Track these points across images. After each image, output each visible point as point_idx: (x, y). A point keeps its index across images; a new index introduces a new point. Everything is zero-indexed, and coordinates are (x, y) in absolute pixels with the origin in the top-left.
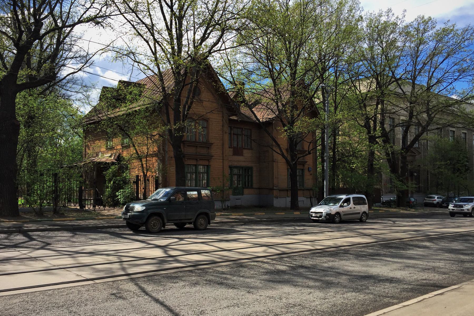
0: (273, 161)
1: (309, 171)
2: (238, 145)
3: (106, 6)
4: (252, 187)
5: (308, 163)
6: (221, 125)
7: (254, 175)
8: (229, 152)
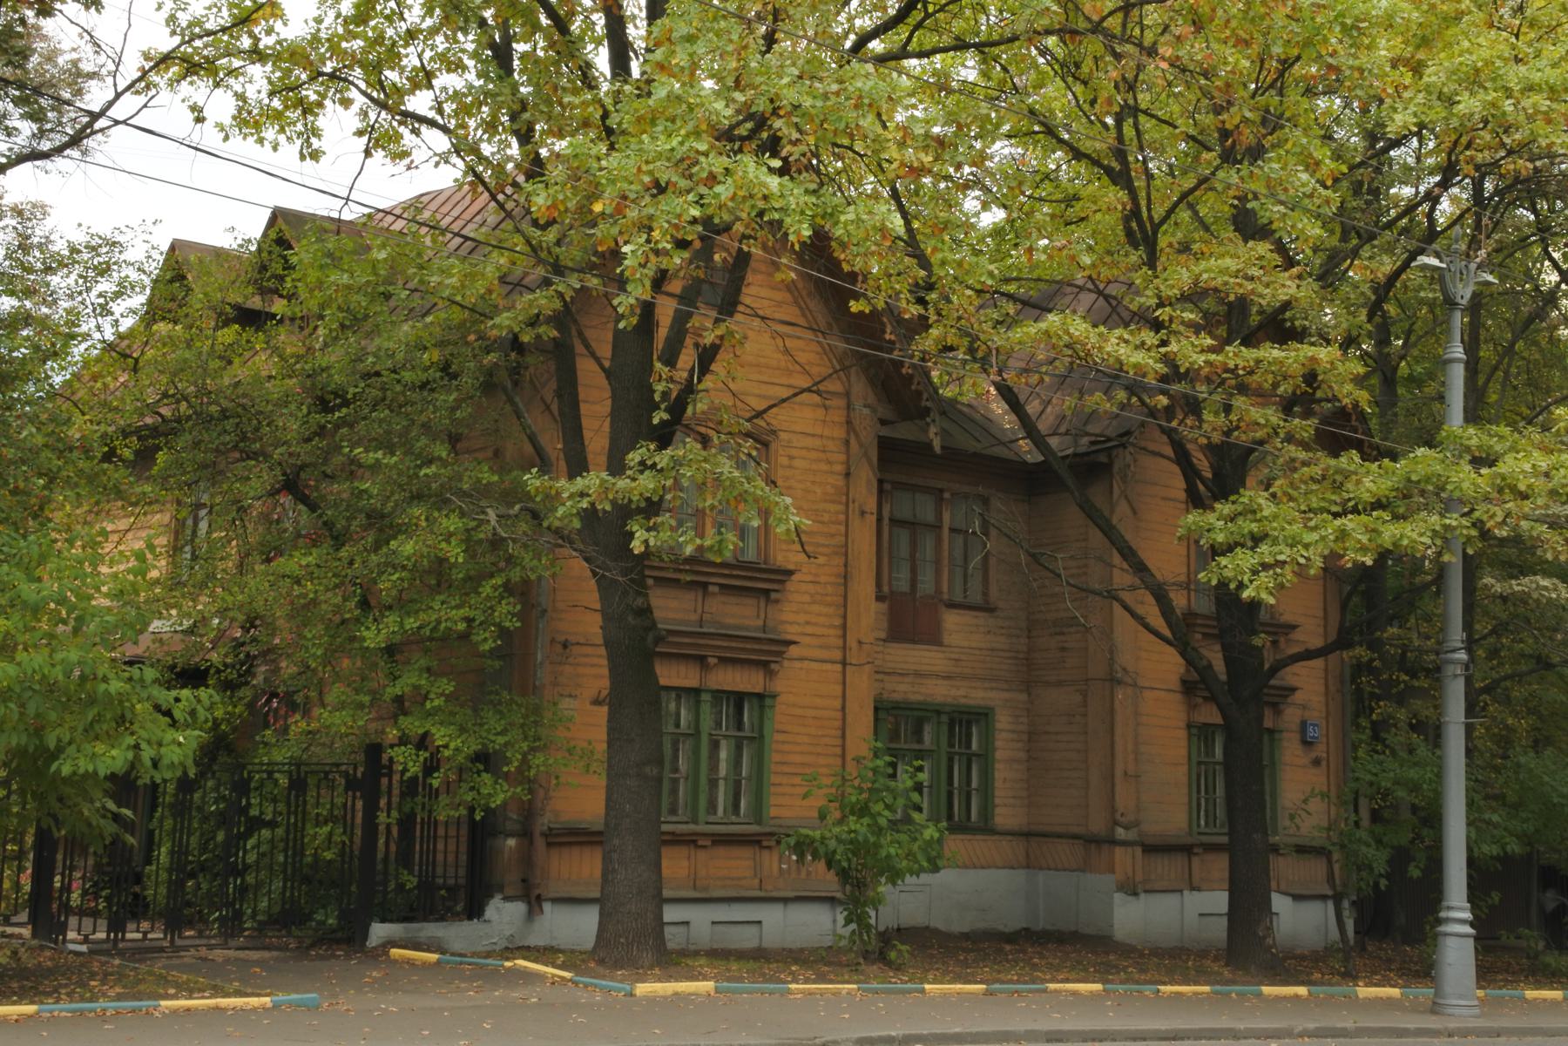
0: (1113, 681)
1: (1307, 743)
2: (914, 583)
3: (1142, 118)
4: (986, 828)
5: (1298, 697)
6: (839, 468)
7: (998, 755)
8: (869, 616)
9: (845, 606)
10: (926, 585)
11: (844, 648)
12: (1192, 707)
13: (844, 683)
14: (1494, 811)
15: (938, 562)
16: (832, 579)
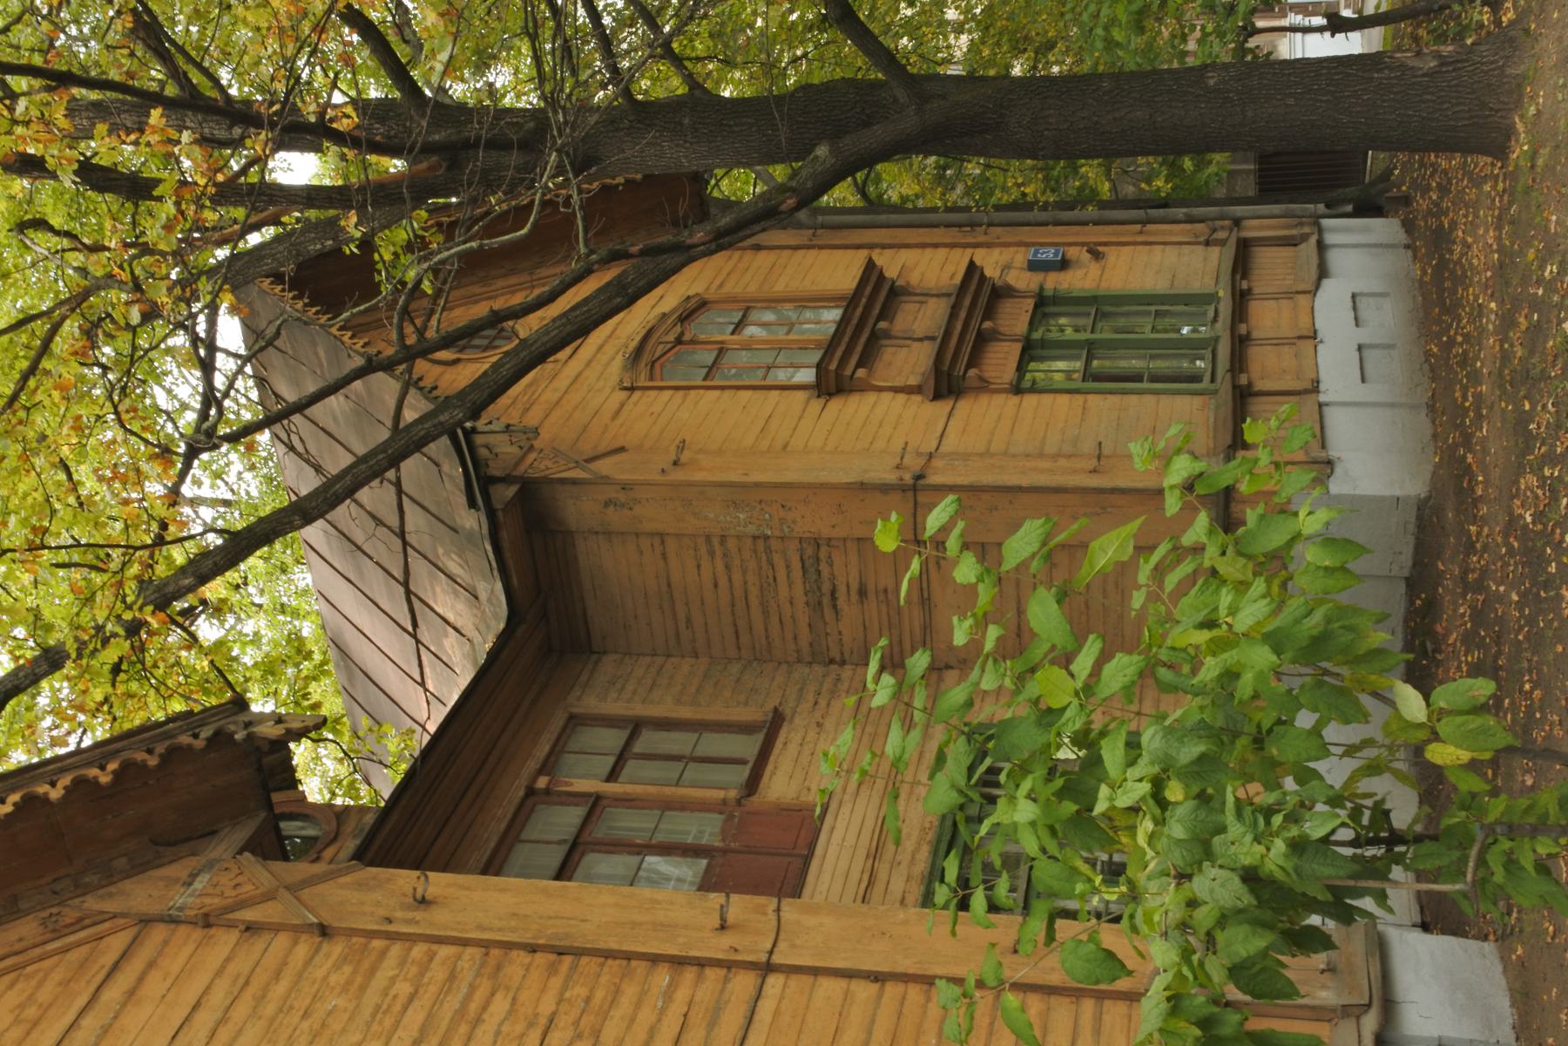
1: (1064, 265)
9: (629, 956)
10: (706, 829)
11: (729, 965)
12: (984, 387)
13: (815, 972)
14: (1324, 987)
15: (667, 805)
16: (556, 983)
